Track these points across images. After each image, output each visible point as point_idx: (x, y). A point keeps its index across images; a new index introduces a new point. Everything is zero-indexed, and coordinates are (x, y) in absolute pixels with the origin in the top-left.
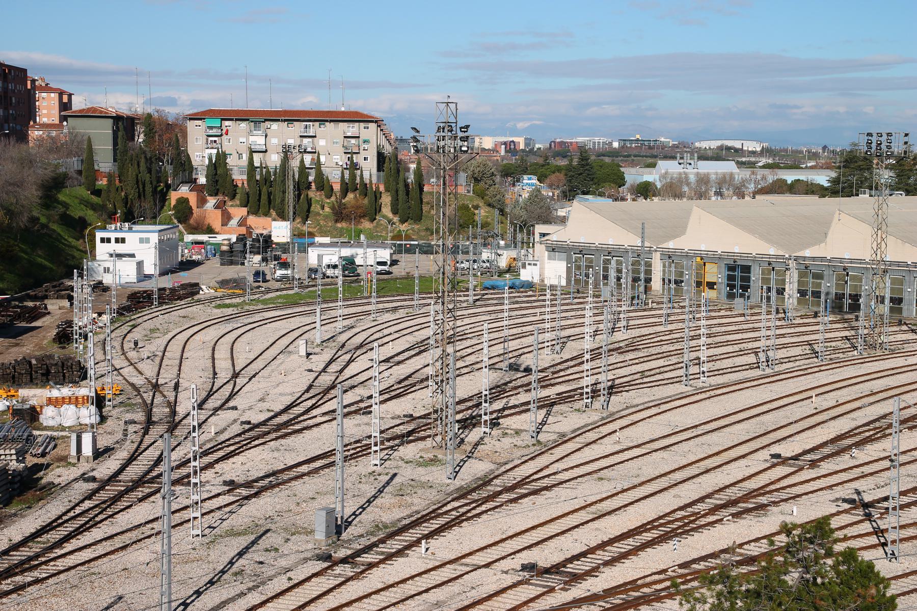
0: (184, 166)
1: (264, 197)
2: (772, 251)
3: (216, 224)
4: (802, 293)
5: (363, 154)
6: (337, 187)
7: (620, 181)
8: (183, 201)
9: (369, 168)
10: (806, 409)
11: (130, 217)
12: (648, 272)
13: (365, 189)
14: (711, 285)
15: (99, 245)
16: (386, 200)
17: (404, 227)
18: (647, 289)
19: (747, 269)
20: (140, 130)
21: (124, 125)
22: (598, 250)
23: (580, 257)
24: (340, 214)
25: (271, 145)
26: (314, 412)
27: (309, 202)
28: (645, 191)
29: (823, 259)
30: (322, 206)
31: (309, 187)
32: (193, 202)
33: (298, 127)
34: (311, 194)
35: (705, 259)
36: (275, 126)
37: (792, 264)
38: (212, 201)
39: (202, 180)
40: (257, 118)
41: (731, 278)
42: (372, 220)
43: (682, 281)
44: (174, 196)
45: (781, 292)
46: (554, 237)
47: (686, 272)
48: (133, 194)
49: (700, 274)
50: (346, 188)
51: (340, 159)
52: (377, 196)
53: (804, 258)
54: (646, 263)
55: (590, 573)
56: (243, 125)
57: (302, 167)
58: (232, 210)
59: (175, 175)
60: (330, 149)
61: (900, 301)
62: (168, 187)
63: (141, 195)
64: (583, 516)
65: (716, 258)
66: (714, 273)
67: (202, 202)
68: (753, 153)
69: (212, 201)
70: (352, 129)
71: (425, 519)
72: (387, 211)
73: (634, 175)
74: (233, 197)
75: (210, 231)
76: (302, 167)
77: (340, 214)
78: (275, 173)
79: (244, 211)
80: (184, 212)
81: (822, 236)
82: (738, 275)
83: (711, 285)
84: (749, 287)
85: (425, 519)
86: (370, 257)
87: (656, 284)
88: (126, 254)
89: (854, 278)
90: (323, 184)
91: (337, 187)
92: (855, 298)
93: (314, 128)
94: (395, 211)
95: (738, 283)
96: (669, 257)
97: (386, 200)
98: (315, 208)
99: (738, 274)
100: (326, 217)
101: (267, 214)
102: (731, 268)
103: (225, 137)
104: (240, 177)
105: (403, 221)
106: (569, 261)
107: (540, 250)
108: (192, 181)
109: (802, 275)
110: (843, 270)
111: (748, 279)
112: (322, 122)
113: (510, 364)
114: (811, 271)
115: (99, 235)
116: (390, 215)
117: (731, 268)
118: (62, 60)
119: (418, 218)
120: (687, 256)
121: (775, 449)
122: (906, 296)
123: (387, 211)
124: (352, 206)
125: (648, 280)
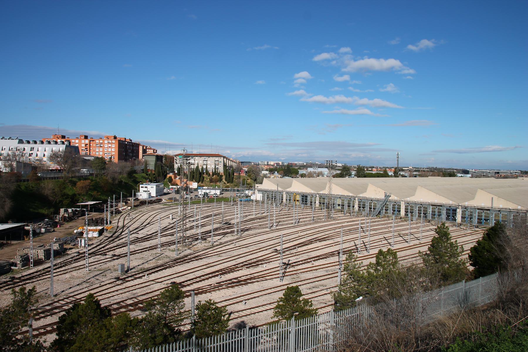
0: (172, 167)
2: (351, 195)
3: (179, 183)
4: (320, 203)
5: (220, 165)
6: (211, 174)
7: (297, 173)
8: (170, 177)
9: (221, 170)
10: (297, 235)
11: (151, 181)
12: (282, 197)
13: (218, 174)
14: (298, 201)
15: (141, 189)
16: (224, 177)
17: (228, 184)
19: (306, 197)
20: (164, 159)
21: (159, 158)
22: (270, 191)
24: (211, 181)
26: (123, 234)
27: (203, 178)
28: (303, 176)
29: (325, 194)
30: (207, 178)
31: (204, 174)
32: (173, 178)
33: (203, 158)
34: (204, 176)
35: (297, 194)
36: (197, 158)
38: (178, 177)
39: (176, 172)
41: (303, 199)
44: (168, 176)
46: (259, 188)
47: (292, 197)
48: (157, 175)
49: (295, 198)
50: (213, 174)
51: (213, 166)
52: (222, 176)
55: (188, 285)
57: (202, 168)
59: (169, 170)
60: (210, 164)
61: (344, 205)
62: (167, 174)
63: (159, 176)
64: (205, 267)
66: (298, 198)
67: (175, 177)
69: (178, 177)
70: (217, 159)
71: (160, 267)
72: (224, 180)
73: (301, 172)
75: (177, 185)
76: (202, 168)
77: (211, 181)
80: (170, 180)
82: (305, 198)
83: (339, 205)
85: (160, 267)
86: (215, 192)
87: (284, 200)
88: (147, 190)
90: (207, 173)
91: (211, 174)
93: (207, 158)
94: (226, 180)
95: (304, 200)
97: (224, 177)
98: (205, 179)
99: (304, 198)
101: (192, 181)
102: (303, 196)
105: (228, 183)
106: (263, 194)
107: (256, 192)
108: (174, 172)
109: (320, 198)
110: (330, 197)
111: (307, 199)
112: (209, 157)
115: (141, 186)
117: (303, 196)
118: (155, 141)
119: (232, 182)
120: (292, 193)
121: (276, 248)
123: (224, 180)
124: (215, 178)
125: (282, 199)
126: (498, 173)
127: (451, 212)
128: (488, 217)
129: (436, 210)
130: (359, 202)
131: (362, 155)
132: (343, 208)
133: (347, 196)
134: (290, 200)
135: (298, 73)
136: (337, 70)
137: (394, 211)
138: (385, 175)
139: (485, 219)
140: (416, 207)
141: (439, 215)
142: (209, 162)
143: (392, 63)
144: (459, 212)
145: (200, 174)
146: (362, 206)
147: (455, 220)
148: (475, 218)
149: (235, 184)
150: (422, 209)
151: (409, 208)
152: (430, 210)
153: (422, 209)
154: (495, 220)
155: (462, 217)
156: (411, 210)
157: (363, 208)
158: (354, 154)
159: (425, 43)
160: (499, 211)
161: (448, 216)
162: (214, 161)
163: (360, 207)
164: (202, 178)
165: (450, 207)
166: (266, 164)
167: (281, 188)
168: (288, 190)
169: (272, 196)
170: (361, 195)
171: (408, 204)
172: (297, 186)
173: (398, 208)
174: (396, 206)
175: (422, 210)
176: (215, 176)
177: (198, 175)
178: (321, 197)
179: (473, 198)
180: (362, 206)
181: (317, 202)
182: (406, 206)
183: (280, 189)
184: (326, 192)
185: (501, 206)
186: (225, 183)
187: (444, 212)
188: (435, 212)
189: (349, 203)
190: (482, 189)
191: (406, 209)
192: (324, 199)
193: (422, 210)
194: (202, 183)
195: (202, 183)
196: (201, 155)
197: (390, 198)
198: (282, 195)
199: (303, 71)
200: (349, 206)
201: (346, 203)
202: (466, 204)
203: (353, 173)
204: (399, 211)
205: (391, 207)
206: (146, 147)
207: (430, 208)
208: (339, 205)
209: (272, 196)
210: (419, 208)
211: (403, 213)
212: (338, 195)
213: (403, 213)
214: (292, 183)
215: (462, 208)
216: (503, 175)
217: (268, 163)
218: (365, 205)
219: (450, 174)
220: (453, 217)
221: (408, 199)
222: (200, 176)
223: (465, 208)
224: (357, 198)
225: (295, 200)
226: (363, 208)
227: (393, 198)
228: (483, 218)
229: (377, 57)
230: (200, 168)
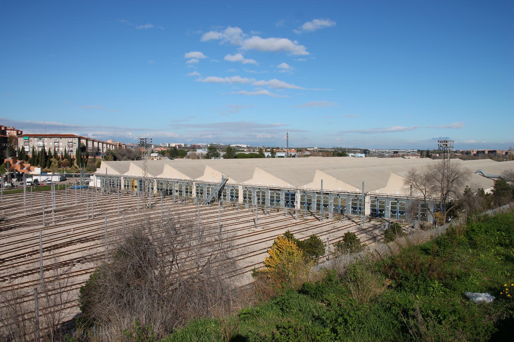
1: (36, 161)
2: (188, 178)
4: (158, 189)
5: (74, 147)
12: (120, 183)
14: (136, 187)
18: (120, 188)
19: (293, 195)
23: (106, 179)
25: (37, 144)
27: (51, 162)
29: (162, 178)
32: (11, 162)
33: (53, 140)
35: (134, 179)
36: (46, 139)
37: (155, 180)
40: (40, 137)
42: (70, 167)
43: (327, 205)
44: (6, 160)
45: (153, 189)
53: (158, 178)
54: (236, 190)
56: (36, 139)
58: (24, 164)
60: (62, 146)
65: (137, 179)
66: (136, 183)
67: (15, 162)
68: (244, 148)
70: (70, 140)
72: (75, 164)
74: (26, 161)
77: (59, 165)
78: (39, 153)
79: (29, 165)
81: (202, 174)
83: (177, 191)
84: (311, 204)
87: (123, 187)
89: (170, 184)
92: (171, 190)
93: (58, 140)
94: (78, 164)
96: (125, 178)
97: (76, 161)
98: (53, 163)
100: (56, 166)
102: (141, 181)
103: (30, 142)
104: (30, 155)
109: (158, 184)
110: (168, 182)
112: (61, 138)
113: (346, 235)
114: (160, 182)
116: (76, 166)
120: (129, 178)
122: (183, 190)
123: (75, 164)
125: (120, 185)
126: (397, 152)
127: (290, 197)
128: (383, 207)
129: (275, 195)
130: (197, 187)
131: (269, 136)
132: (181, 194)
133: (185, 180)
134: (128, 186)
135: (188, 52)
136: (233, 49)
137: (232, 197)
138: (261, 155)
139: (324, 205)
140: (254, 192)
141: (278, 201)
142: (61, 144)
143: (283, 42)
144: (298, 197)
145: (72, 160)
146: (199, 192)
147: (294, 206)
148: (314, 203)
149: (88, 168)
150: (261, 194)
151: (247, 193)
152: (314, 200)
153: (261, 194)
154: (334, 205)
155: (301, 203)
156: (249, 195)
157: (201, 193)
158: (260, 135)
159: (319, 23)
160: (338, 195)
161: (287, 202)
162: (66, 143)
163: (198, 193)
164: (48, 163)
165: (288, 191)
166: (168, 146)
167: (151, 173)
168: (126, 174)
169: (110, 182)
170: (198, 179)
171: (246, 187)
172: (134, 170)
173: (277, 197)
174: (234, 191)
175: (261, 196)
176: (65, 160)
177: (44, 160)
178: (158, 182)
179: (251, 177)
180: (199, 192)
181: (155, 188)
182: (244, 191)
183: (149, 176)
184: (314, 186)
185: (340, 189)
186: (76, 168)
187: (283, 197)
188: (395, 208)
189: (187, 189)
190: (321, 170)
191: (372, 206)
192: (161, 184)
193: (261, 196)
194: (49, 168)
195: (49, 168)
196: (51, 136)
197: (228, 182)
198: (120, 180)
199: (199, 51)
200: (187, 192)
201: (184, 189)
202: (305, 187)
203: (222, 154)
204: (237, 197)
205: (228, 192)
206: (5, 128)
207: (268, 192)
208: (177, 191)
209: (110, 182)
210: (232, 190)
211: (241, 199)
212: (176, 179)
213: (241, 199)
214: (129, 166)
215: (301, 192)
216: (400, 154)
217: (169, 145)
218: (310, 200)
219: (341, 153)
220: (293, 202)
221: (246, 183)
222: (46, 161)
223: (304, 192)
224: (194, 183)
225: (133, 186)
226: (201, 193)
227: (231, 181)
228: (398, 209)
229: (264, 37)
230: (47, 149)
